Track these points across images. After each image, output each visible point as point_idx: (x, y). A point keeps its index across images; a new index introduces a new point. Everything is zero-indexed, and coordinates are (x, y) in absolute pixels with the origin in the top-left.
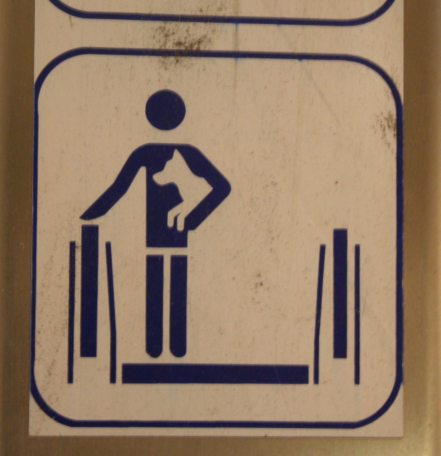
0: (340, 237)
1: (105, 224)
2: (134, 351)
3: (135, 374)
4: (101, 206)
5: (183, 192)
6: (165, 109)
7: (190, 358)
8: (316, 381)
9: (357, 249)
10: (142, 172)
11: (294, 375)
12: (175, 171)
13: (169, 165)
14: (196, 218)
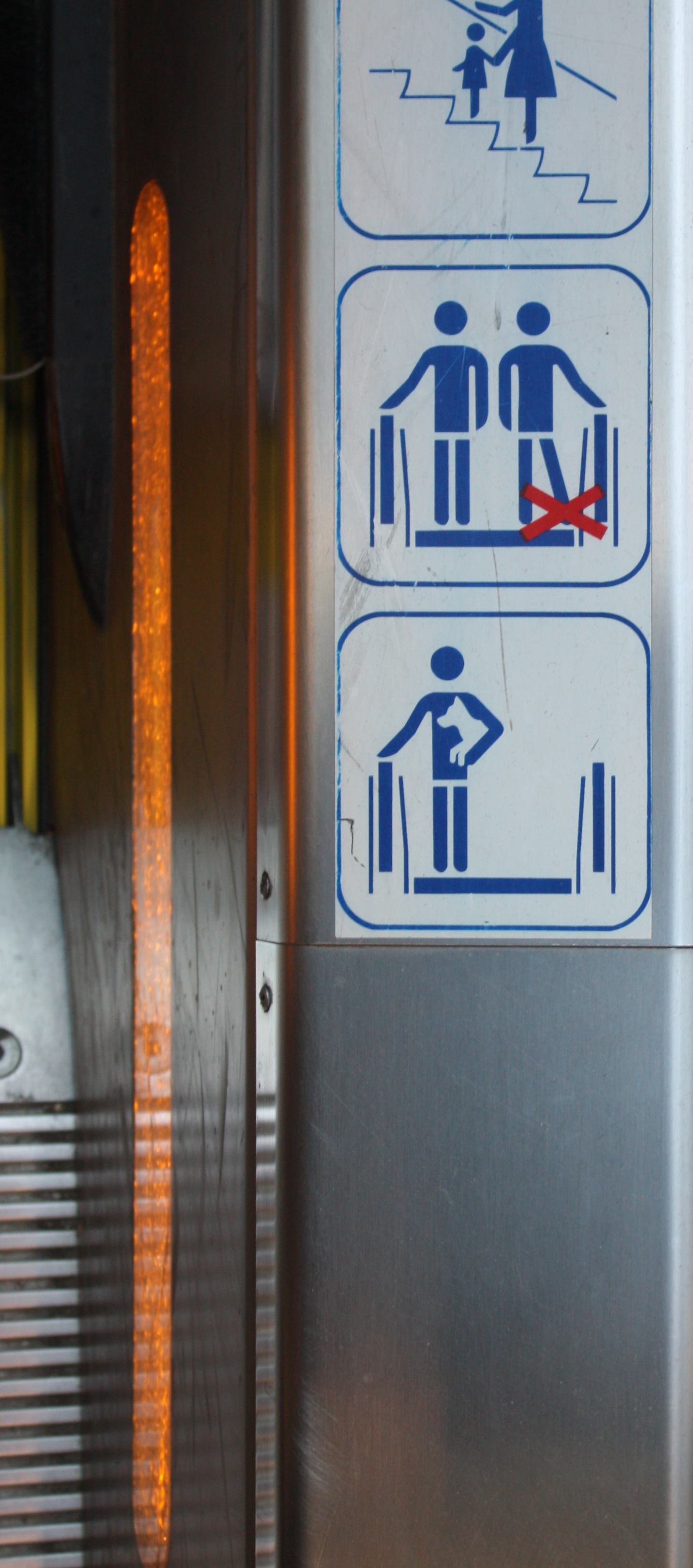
0: (598, 770)
1: (398, 414)
2: (423, 866)
3: (424, 886)
4: (395, 400)
5: (462, 734)
6: (447, 662)
7: (472, 872)
8: (578, 891)
9: (616, 431)
10: (428, 716)
11: (560, 886)
12: (457, 716)
13: (451, 709)
14: (474, 755)
